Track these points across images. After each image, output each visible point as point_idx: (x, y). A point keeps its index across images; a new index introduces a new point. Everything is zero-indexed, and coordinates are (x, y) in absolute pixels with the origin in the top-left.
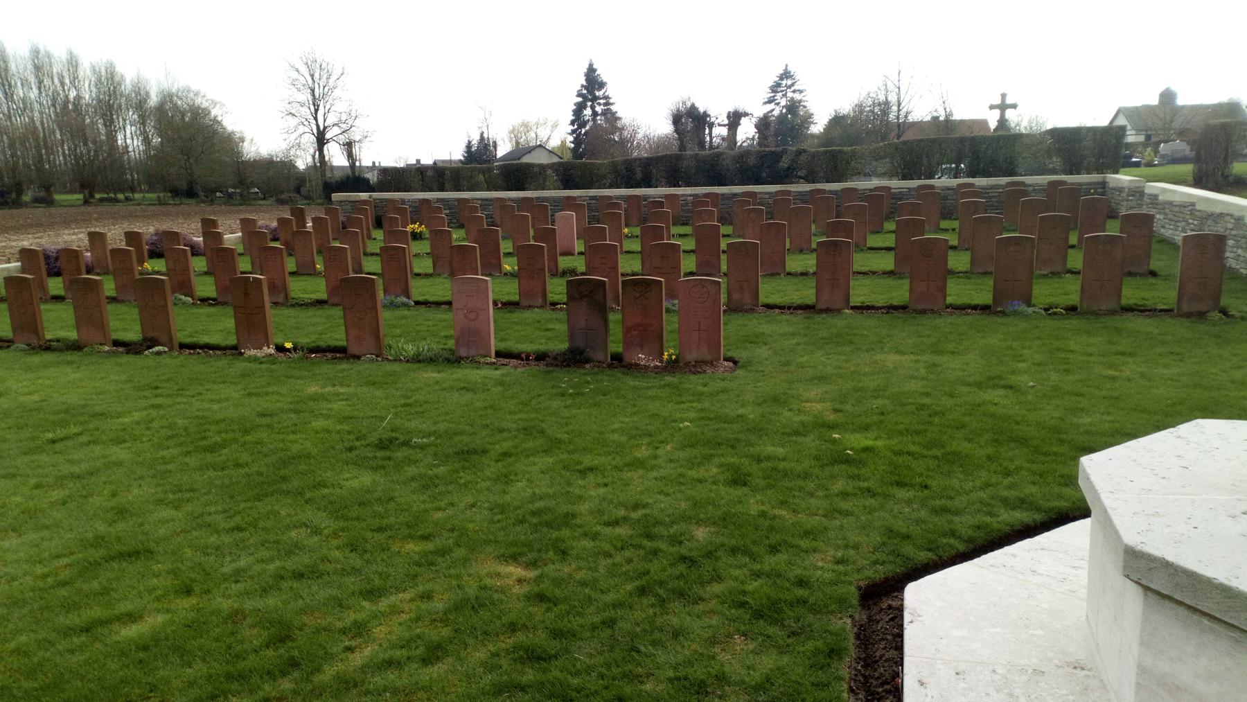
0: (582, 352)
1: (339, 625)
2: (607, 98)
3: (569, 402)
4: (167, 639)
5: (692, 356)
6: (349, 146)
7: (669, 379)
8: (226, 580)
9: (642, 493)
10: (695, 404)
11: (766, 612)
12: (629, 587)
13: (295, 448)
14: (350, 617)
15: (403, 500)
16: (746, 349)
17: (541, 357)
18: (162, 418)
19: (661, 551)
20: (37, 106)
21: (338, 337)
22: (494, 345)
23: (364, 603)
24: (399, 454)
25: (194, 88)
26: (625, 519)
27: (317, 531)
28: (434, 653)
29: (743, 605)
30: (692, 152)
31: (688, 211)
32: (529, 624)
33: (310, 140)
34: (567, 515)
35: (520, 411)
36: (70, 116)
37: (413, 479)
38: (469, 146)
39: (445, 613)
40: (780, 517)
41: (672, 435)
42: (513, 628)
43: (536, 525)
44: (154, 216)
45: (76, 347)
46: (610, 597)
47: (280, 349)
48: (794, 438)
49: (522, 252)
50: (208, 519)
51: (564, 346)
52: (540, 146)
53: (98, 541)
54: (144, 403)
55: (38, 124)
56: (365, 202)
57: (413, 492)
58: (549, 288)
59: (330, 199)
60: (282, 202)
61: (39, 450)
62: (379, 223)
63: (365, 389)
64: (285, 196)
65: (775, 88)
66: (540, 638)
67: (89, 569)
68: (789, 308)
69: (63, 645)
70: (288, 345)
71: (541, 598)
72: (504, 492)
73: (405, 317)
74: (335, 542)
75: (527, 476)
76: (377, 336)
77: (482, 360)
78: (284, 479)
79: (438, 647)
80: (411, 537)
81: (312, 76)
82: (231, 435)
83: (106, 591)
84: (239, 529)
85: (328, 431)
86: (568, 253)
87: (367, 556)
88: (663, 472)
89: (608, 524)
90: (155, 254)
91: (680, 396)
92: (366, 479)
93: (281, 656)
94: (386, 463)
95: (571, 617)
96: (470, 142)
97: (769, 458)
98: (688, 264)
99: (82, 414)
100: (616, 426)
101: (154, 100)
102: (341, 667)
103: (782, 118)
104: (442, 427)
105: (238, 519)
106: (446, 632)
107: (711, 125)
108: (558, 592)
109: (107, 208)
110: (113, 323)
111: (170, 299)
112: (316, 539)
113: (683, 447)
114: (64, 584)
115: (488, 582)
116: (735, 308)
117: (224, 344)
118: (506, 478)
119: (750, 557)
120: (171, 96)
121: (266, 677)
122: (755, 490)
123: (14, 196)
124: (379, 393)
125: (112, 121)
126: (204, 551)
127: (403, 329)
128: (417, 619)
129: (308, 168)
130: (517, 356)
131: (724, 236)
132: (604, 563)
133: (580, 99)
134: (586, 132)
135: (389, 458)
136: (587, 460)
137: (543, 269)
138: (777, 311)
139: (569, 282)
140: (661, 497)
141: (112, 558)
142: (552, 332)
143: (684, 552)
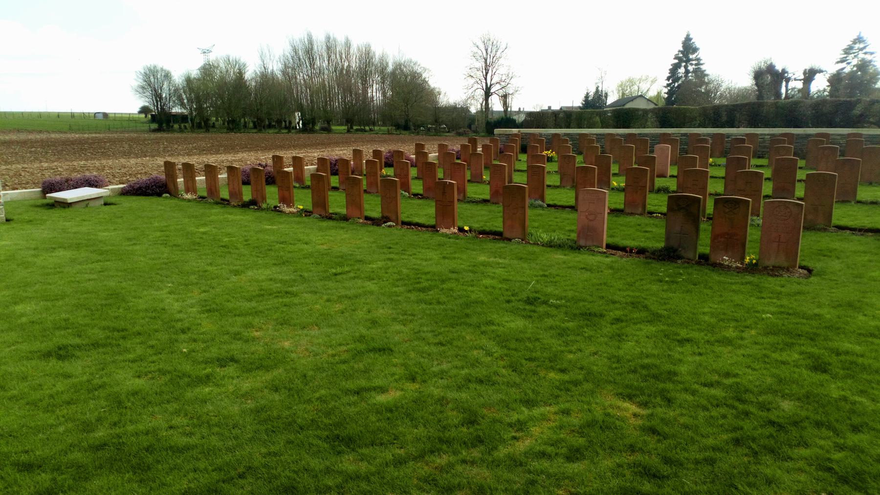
0: (676, 251)
1: (508, 420)
2: (698, 59)
3: (665, 287)
4: (403, 408)
5: (770, 262)
6: (505, 97)
7: (749, 278)
8: (435, 376)
9: (732, 364)
10: (775, 301)
11: (851, 478)
12: (725, 437)
13: (473, 296)
14: (515, 417)
15: (545, 341)
16: (820, 260)
17: (641, 251)
18: (394, 267)
19: (752, 413)
20: (326, 72)
21: (498, 225)
22: (606, 240)
23: (524, 409)
24: (541, 309)
25: (414, 60)
26: (719, 383)
27: (489, 354)
28: (575, 454)
29: (829, 470)
30: (768, 103)
31: (765, 147)
32: (645, 449)
33: (480, 93)
34: (669, 373)
35: (627, 290)
36: (343, 77)
37: (551, 328)
38: (587, 97)
39: (580, 428)
40: (860, 403)
41: (756, 323)
42: (632, 449)
43: (646, 376)
44: (385, 141)
45: (345, 218)
46: (710, 441)
47: (461, 230)
48: (870, 339)
49: (627, 172)
50: (423, 335)
51: (661, 245)
52: (641, 96)
53: (362, 339)
54: (383, 257)
55: (326, 83)
56: (516, 135)
57: (551, 337)
58: (648, 201)
59: (493, 133)
60: (459, 134)
61: (327, 278)
62: (524, 150)
63: (515, 262)
64: (461, 130)
65: (848, 51)
66: (654, 461)
67: (358, 354)
68: (860, 230)
69: (345, 399)
70: (466, 228)
71: (653, 431)
72: (619, 348)
73: (540, 215)
74: (502, 363)
75: (635, 338)
76: (523, 227)
77: (596, 250)
78: (467, 315)
79: (578, 450)
80: (552, 368)
81: (487, 50)
82: (433, 283)
83: (366, 371)
84: (442, 344)
85: (494, 288)
86: (662, 176)
87: (523, 376)
88: (748, 351)
89: (705, 385)
90: (388, 165)
91: (761, 292)
92: (518, 323)
93: (471, 434)
94: (532, 314)
95: (678, 450)
96: (588, 94)
97: (847, 353)
98: (767, 188)
99: (350, 260)
100: (706, 310)
101: (390, 68)
102: (510, 450)
103: (852, 74)
104: (570, 294)
105: (441, 337)
106: (582, 441)
107: (788, 80)
108: (666, 429)
109: (359, 135)
110: (366, 206)
111: (528, 201)
112: (489, 359)
113: (767, 334)
114: (344, 362)
115: (610, 411)
116: (810, 227)
117: (427, 223)
118: (619, 337)
119: (834, 432)
120: (400, 65)
121: (463, 446)
122: (835, 377)
123: (311, 126)
124: (525, 265)
125: (366, 81)
126: (421, 354)
127: (541, 223)
128: (561, 427)
129: (477, 112)
130: (623, 249)
131: (800, 168)
132: (702, 414)
133: (677, 61)
134: (679, 85)
135: (534, 311)
136: (683, 333)
137: (645, 187)
138: (848, 232)
139: (670, 197)
140: (750, 371)
141: (371, 351)
142: (653, 235)
143: (773, 417)
